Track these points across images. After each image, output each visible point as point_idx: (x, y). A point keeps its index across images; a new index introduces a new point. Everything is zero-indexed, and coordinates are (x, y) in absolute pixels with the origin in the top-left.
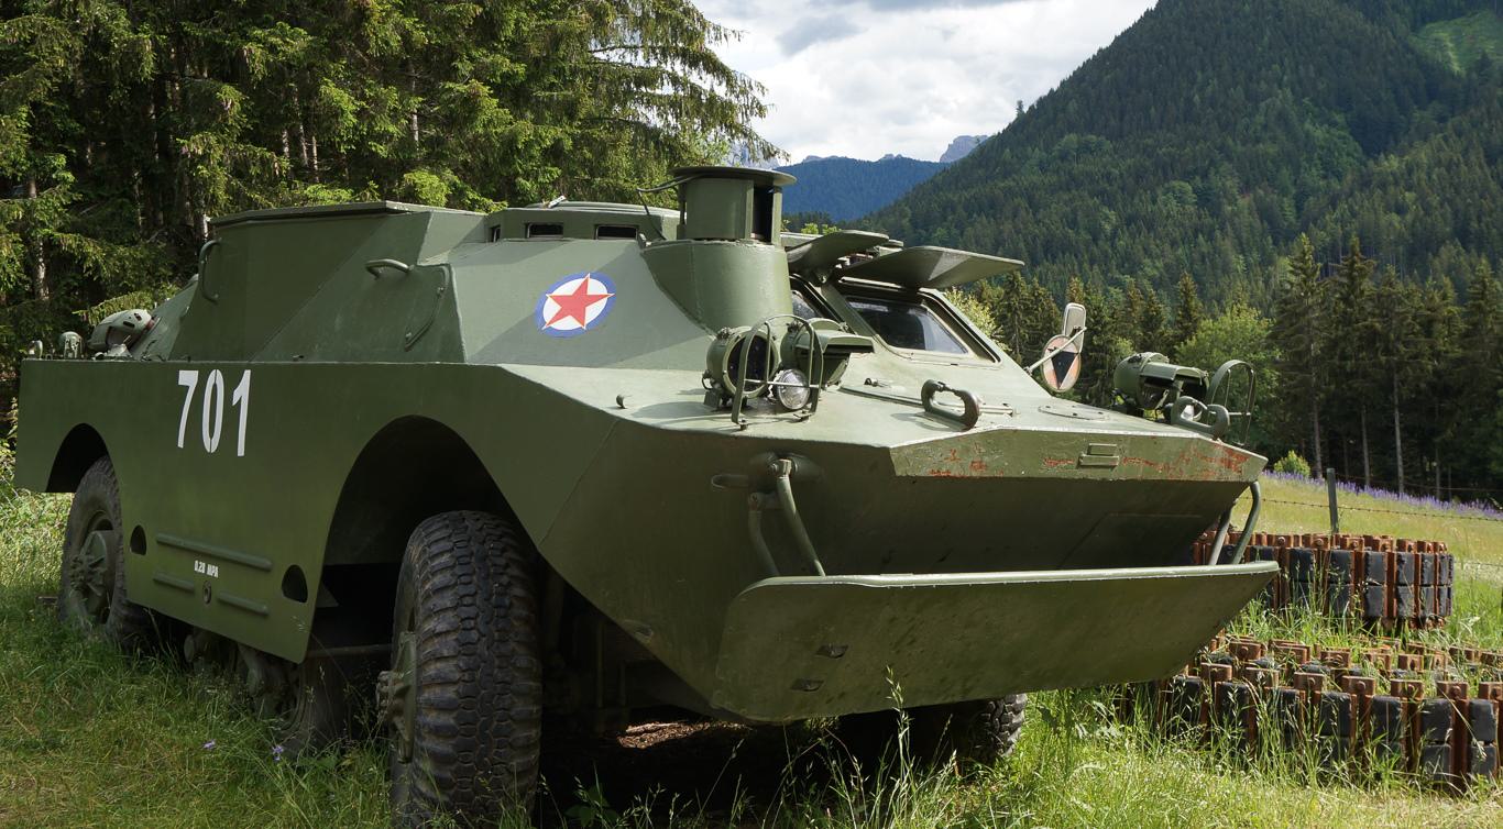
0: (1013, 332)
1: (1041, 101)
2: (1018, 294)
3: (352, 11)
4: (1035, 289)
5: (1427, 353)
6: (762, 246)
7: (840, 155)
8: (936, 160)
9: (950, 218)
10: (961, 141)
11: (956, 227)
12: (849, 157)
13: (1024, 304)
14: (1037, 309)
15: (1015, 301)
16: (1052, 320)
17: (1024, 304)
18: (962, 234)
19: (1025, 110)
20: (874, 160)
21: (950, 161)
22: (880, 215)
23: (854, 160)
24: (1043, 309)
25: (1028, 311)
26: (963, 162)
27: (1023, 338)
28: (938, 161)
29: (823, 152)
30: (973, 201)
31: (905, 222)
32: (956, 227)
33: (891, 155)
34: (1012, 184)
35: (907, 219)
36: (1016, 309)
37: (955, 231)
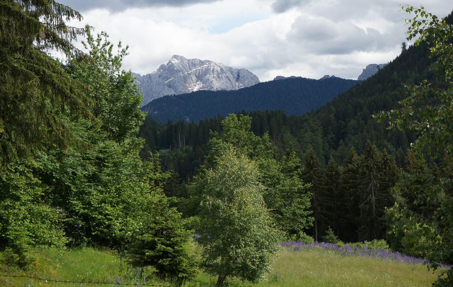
0: (370, 182)
1: (452, 12)
2: (373, 158)
3: (451, 266)
4: (385, 156)
5: (252, 177)
6: (59, 58)
7: (297, 75)
8: (356, 79)
9: (359, 114)
10: (371, 67)
11: (362, 119)
12: (303, 77)
13: (377, 165)
14: (385, 169)
15: (370, 163)
16: (394, 175)
17: (377, 165)
18: (366, 123)
19: (407, 48)
20: (317, 79)
21: (363, 79)
22: (318, 111)
23: (305, 79)
24: (390, 168)
25: (379, 169)
26: (369, 80)
27: (375, 186)
28: (356, 79)
29: (286, 73)
30: (373, 103)
31: (332, 116)
32: (362, 119)
33: (328, 76)
34: (398, 93)
35: (333, 114)
36: (371, 168)
37: (362, 122)
